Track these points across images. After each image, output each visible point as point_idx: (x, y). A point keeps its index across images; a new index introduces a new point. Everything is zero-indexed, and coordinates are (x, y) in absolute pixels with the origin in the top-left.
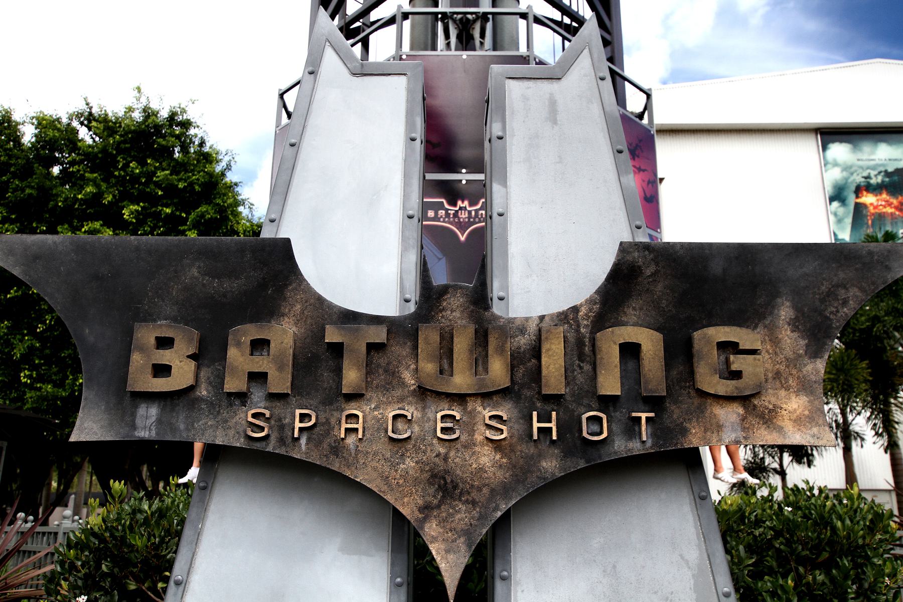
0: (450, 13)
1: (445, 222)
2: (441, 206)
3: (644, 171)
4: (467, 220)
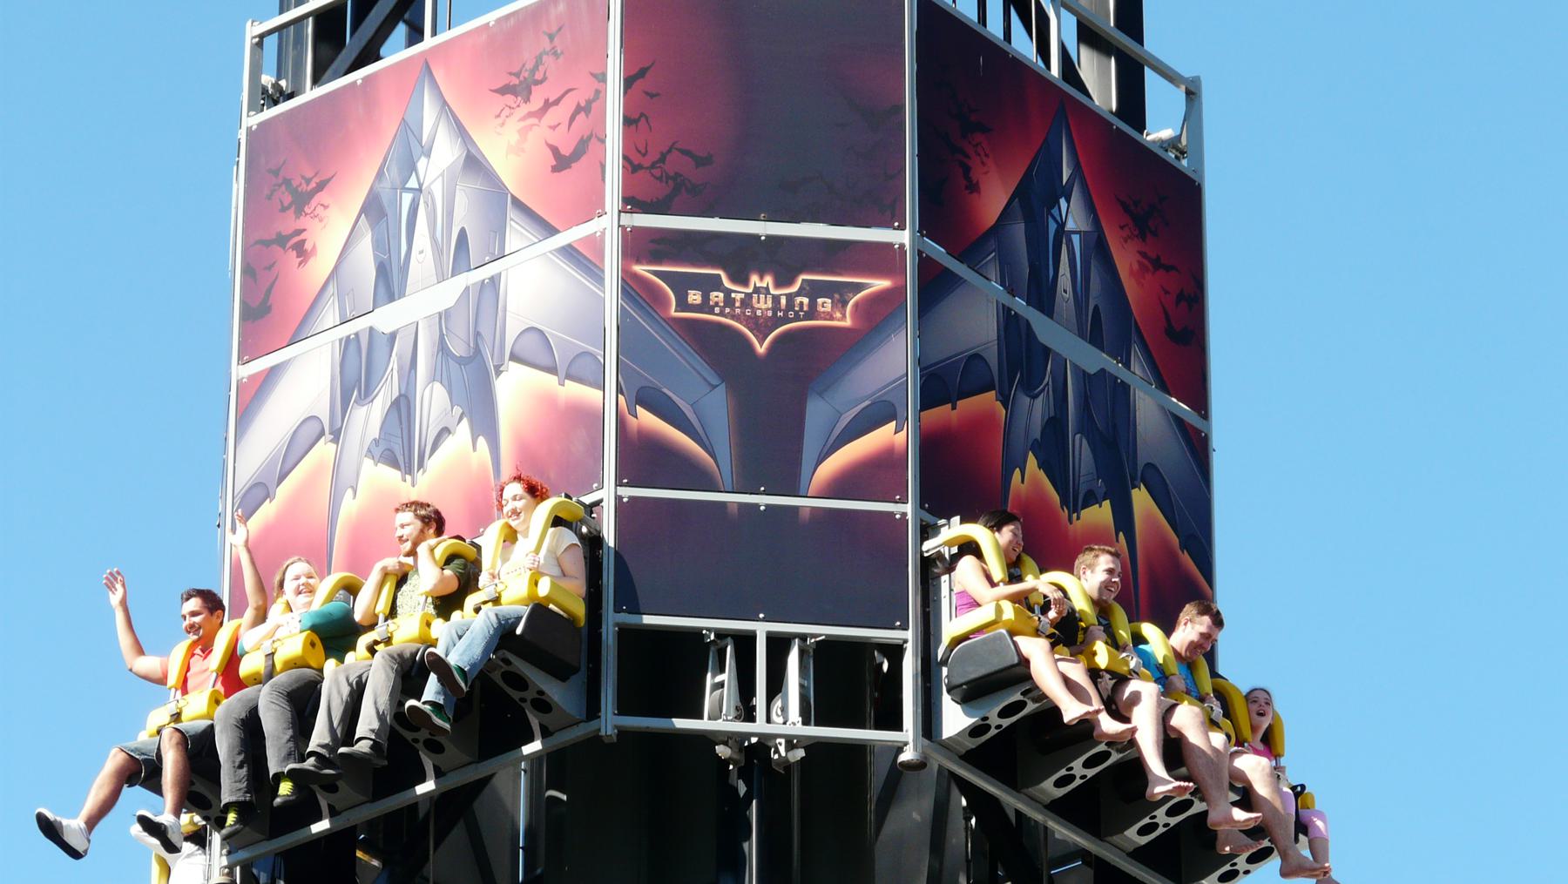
1: (733, 317)
2: (716, 283)
3: (1168, 268)
4: (770, 313)
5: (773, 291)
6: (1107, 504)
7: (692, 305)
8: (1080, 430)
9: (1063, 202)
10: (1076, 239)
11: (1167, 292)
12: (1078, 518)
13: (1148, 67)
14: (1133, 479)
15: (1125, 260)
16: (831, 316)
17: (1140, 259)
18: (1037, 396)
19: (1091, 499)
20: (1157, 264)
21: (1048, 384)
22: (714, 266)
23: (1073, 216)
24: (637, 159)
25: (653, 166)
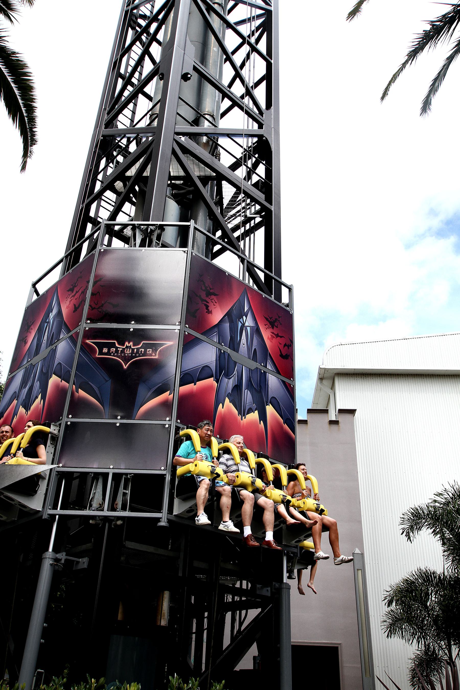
0: (137, 224)
1: (117, 357)
2: (113, 345)
3: (281, 337)
4: (130, 355)
5: (132, 347)
6: (256, 412)
7: (104, 353)
8: (247, 388)
9: (244, 317)
10: (248, 328)
11: (280, 344)
12: (245, 418)
13: (106, 159)
14: (267, 402)
15: (266, 334)
16: (151, 355)
17: (272, 334)
18: (230, 378)
19: (250, 411)
20: (277, 336)
21: (235, 374)
22: (113, 340)
23: (249, 322)
24: (93, 306)
25: (99, 308)
